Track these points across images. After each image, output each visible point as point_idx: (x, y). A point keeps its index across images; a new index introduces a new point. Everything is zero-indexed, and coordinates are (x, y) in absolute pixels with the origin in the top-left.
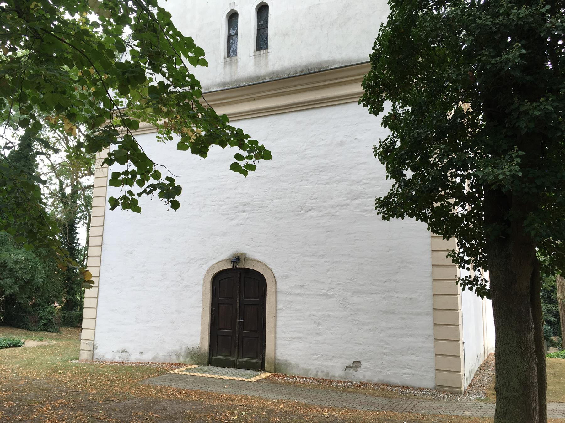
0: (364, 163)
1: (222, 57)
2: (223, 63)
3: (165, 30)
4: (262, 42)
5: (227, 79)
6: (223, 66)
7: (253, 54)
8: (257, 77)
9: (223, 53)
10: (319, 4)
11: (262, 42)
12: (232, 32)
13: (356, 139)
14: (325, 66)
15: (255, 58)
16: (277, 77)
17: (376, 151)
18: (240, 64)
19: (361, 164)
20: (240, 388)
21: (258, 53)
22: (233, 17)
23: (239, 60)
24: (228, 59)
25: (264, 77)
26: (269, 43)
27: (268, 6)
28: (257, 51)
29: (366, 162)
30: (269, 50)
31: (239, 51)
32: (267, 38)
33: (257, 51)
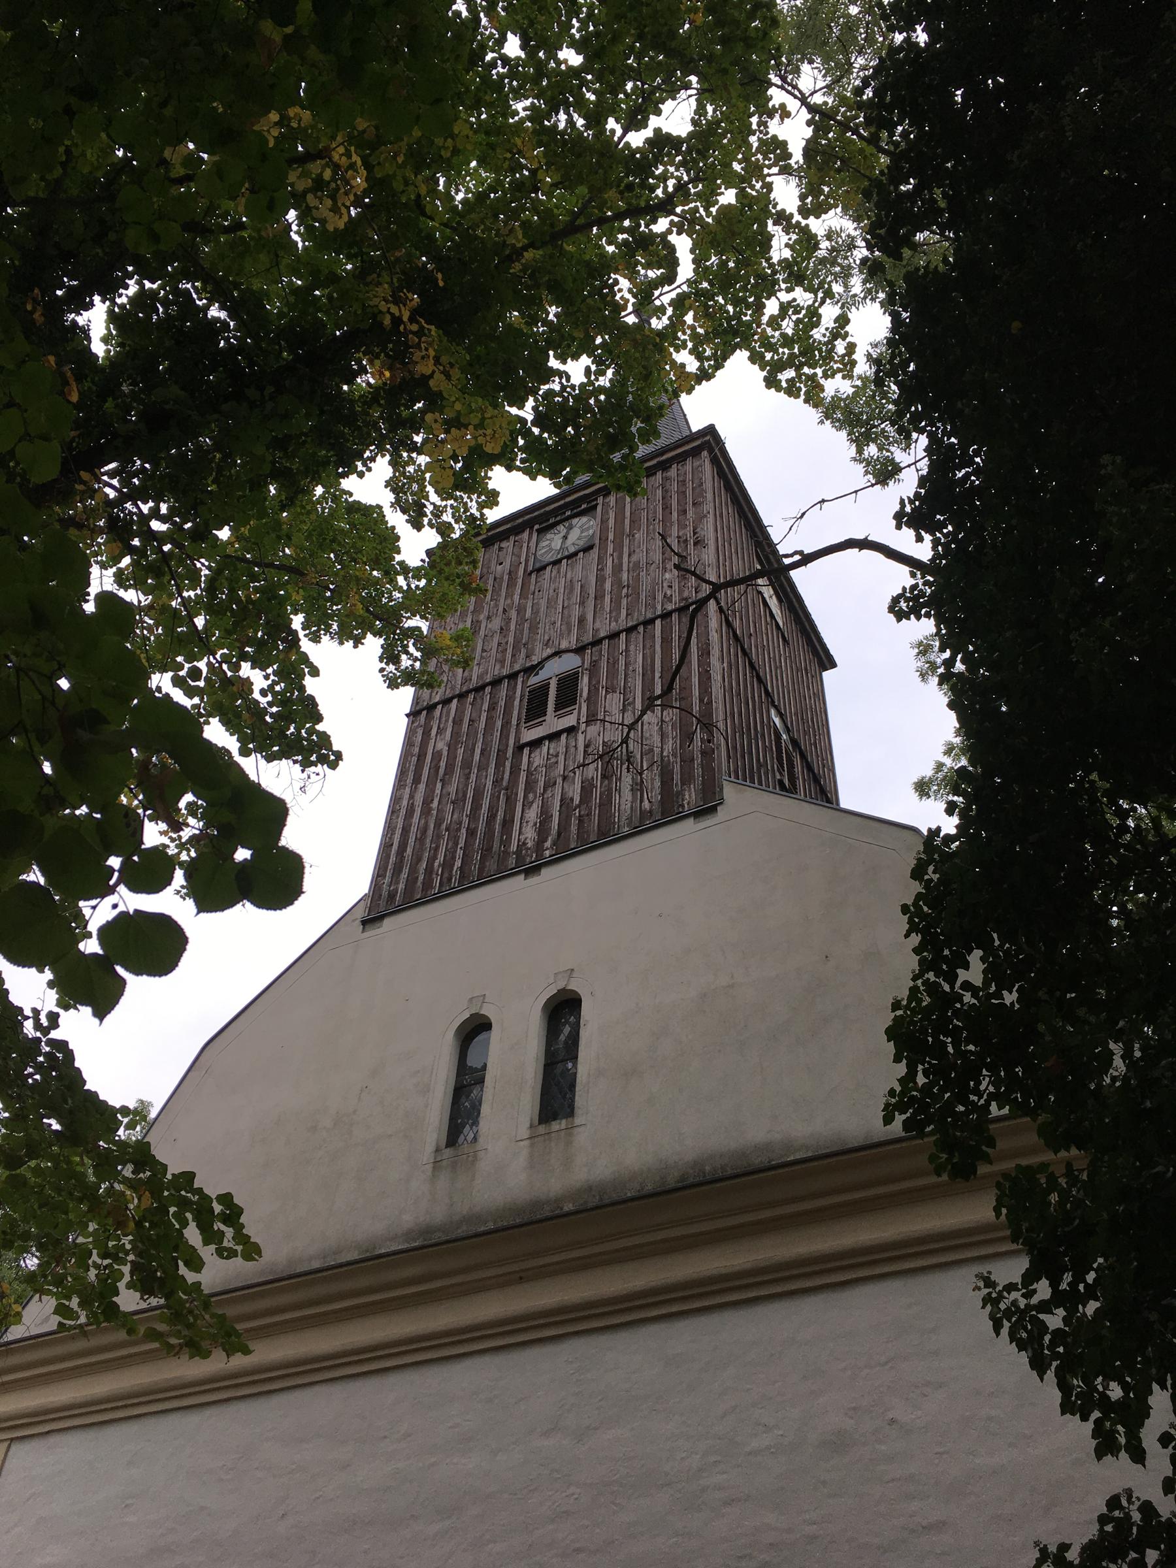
0: (939, 1526)
1: (430, 1148)
2: (429, 1167)
3: (341, 470)
4: (557, 1097)
5: (439, 1214)
6: (429, 1173)
7: (524, 1132)
8: (536, 1204)
9: (435, 1136)
10: (732, 986)
11: (557, 1097)
12: (473, 1061)
13: (893, 1421)
14: (757, 1161)
15: (532, 1145)
16: (601, 1199)
17: (995, 1302)
18: (485, 1165)
19: (928, 1528)
20: (490, 849)
21: (542, 1129)
22: (475, 1029)
23: (481, 1154)
24: (448, 1152)
25: (558, 1201)
26: (579, 1100)
27: (580, 1000)
28: (540, 1123)
29: (944, 1523)
30: (578, 1120)
31: (485, 1109)
32: (572, 1086)
33: (540, 1123)
